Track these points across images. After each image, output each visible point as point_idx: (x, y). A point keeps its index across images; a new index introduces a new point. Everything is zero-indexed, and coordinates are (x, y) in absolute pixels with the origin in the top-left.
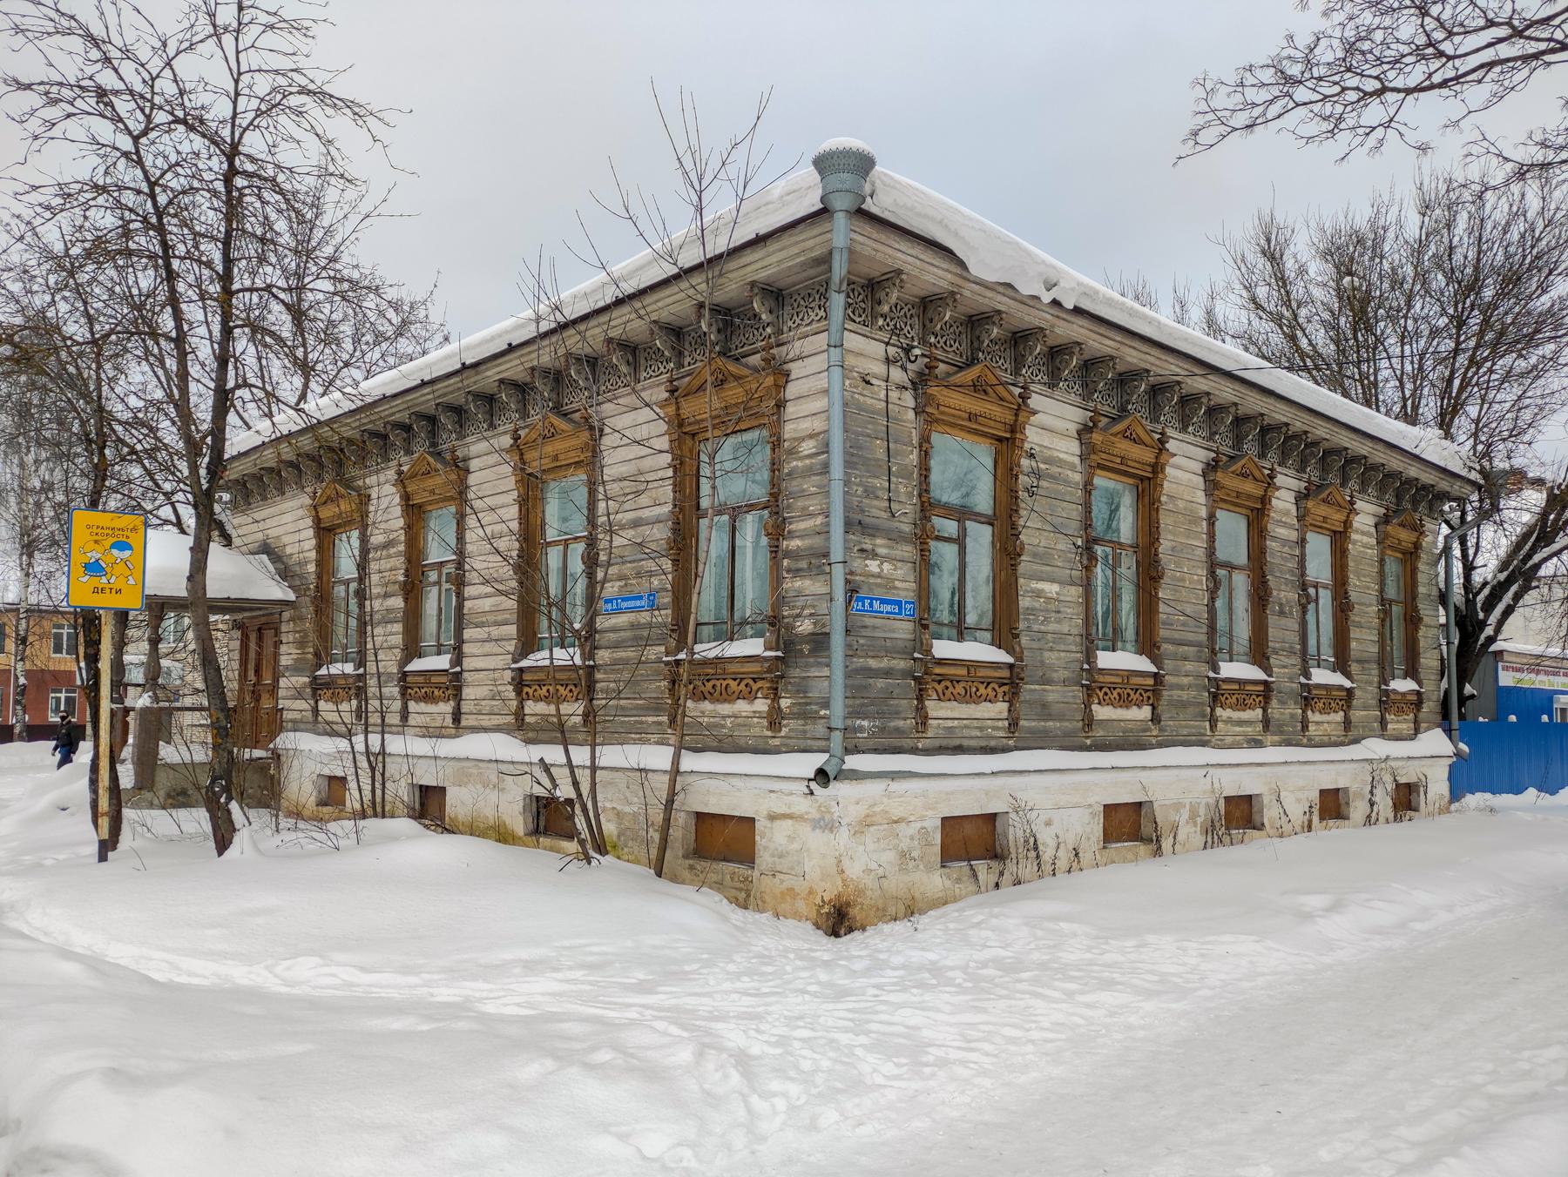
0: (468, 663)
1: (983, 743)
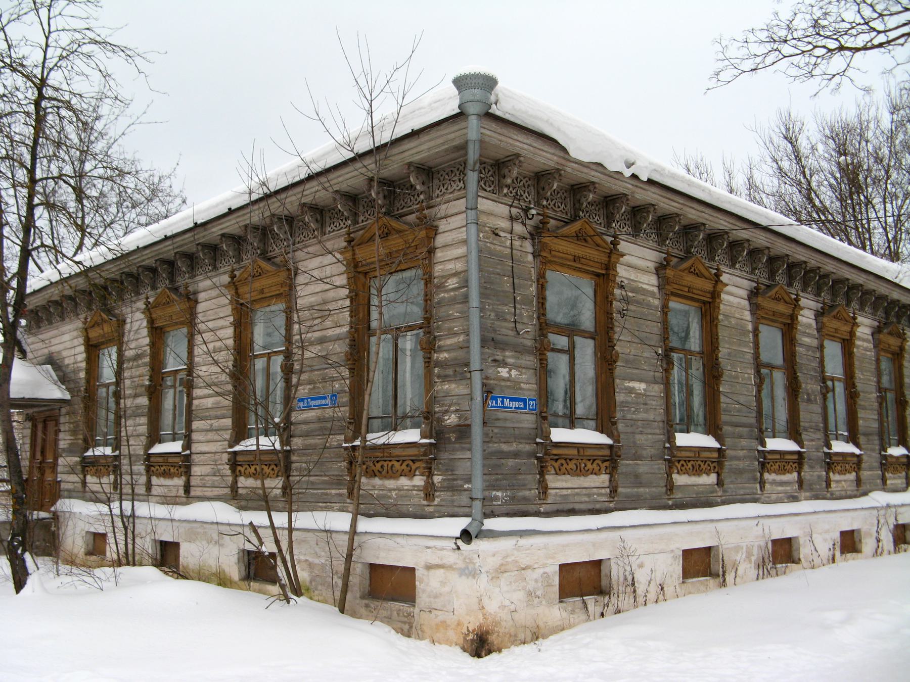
0: (196, 447)
1: (590, 506)
